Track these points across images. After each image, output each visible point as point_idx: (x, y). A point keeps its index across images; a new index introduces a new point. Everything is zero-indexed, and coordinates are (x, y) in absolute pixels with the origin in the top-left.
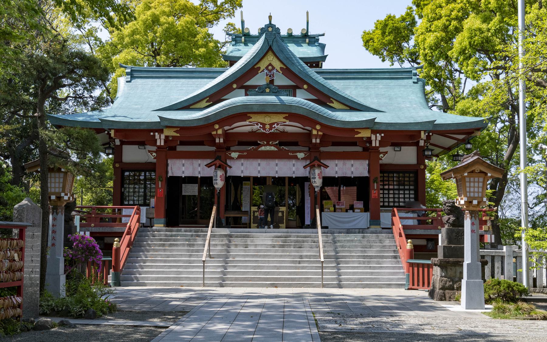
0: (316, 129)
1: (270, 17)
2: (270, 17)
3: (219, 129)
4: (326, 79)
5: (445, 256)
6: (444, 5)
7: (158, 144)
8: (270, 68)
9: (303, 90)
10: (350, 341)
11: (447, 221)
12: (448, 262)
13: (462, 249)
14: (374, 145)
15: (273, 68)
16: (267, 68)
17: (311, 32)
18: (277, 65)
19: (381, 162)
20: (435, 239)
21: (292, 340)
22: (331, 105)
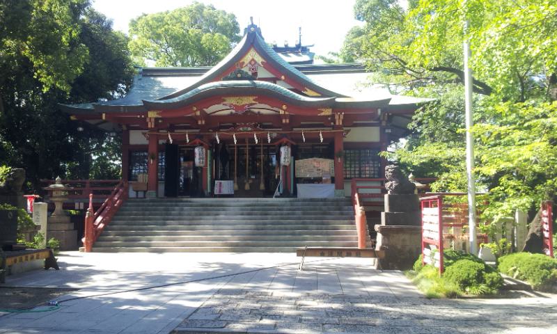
0: (282, 109)
1: (251, 18)
2: (251, 18)
3: (197, 110)
4: (305, 73)
5: (387, 223)
6: (473, 75)
7: (149, 126)
8: (253, 63)
9: (282, 82)
10: (466, 330)
11: (389, 187)
12: (391, 229)
13: (384, 202)
14: (337, 124)
15: (256, 62)
16: (250, 63)
17: (303, 45)
18: (259, 59)
19: (345, 140)
20: (260, 150)
21: (460, 333)
22: (305, 92)
